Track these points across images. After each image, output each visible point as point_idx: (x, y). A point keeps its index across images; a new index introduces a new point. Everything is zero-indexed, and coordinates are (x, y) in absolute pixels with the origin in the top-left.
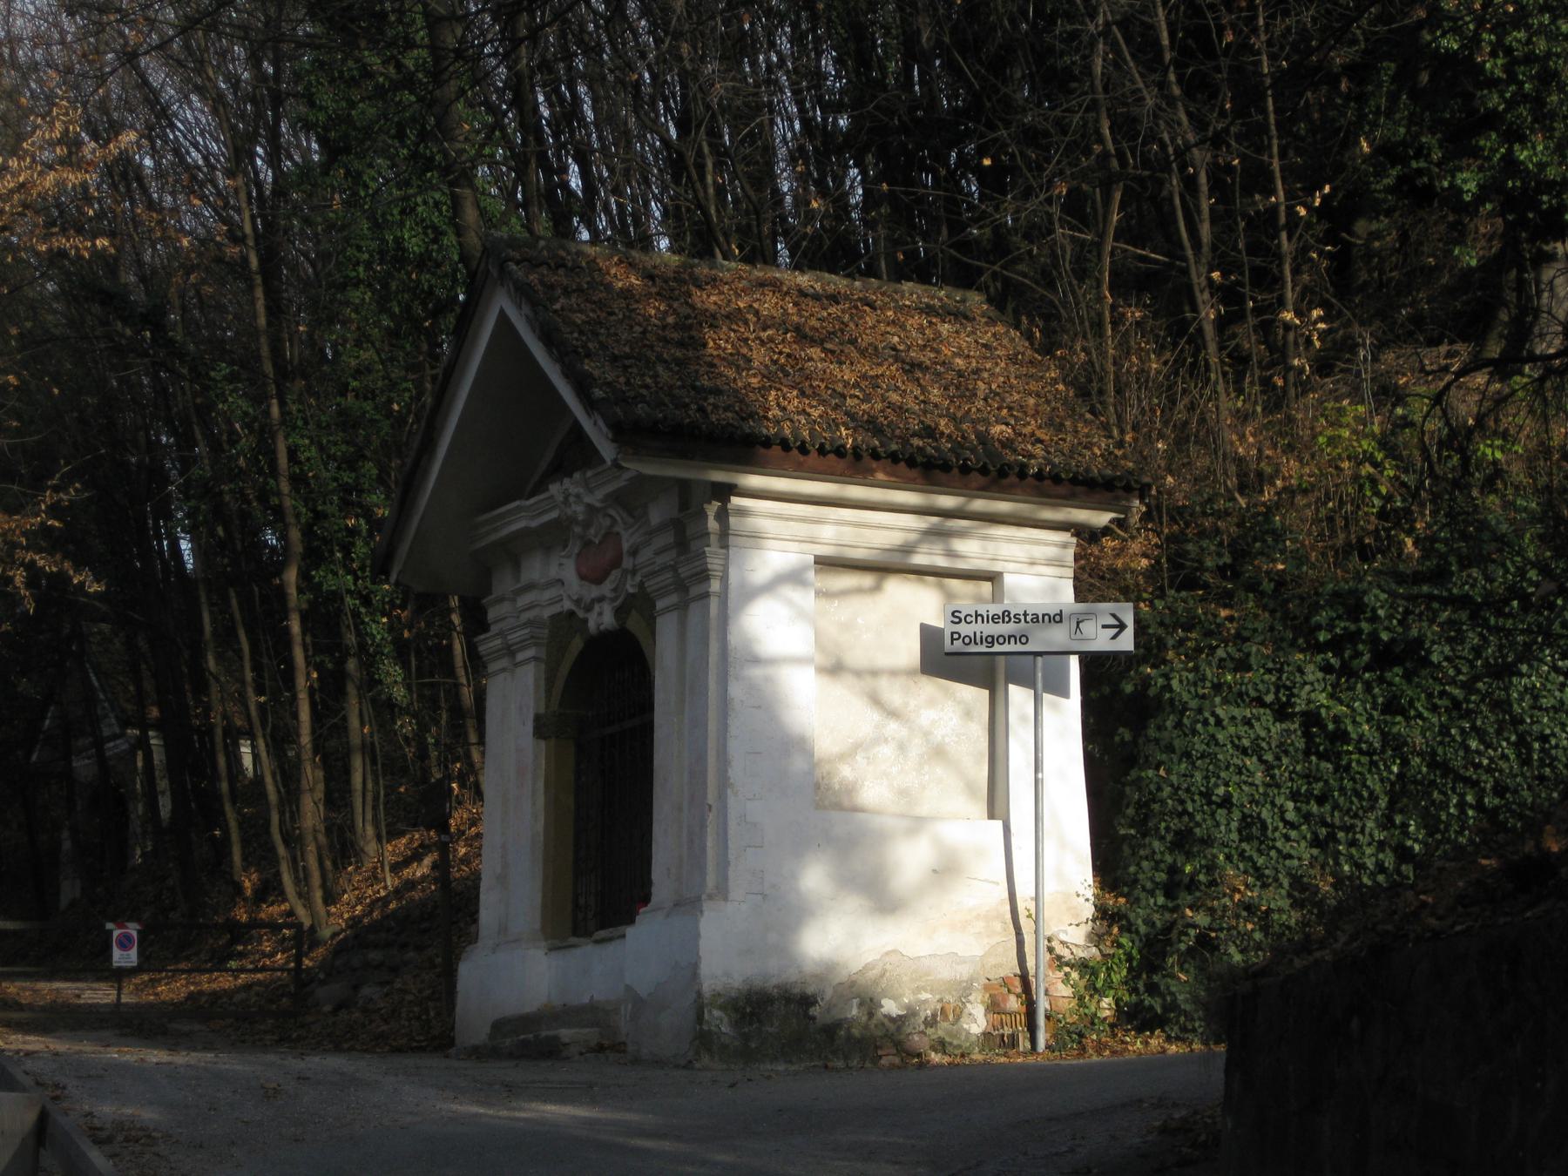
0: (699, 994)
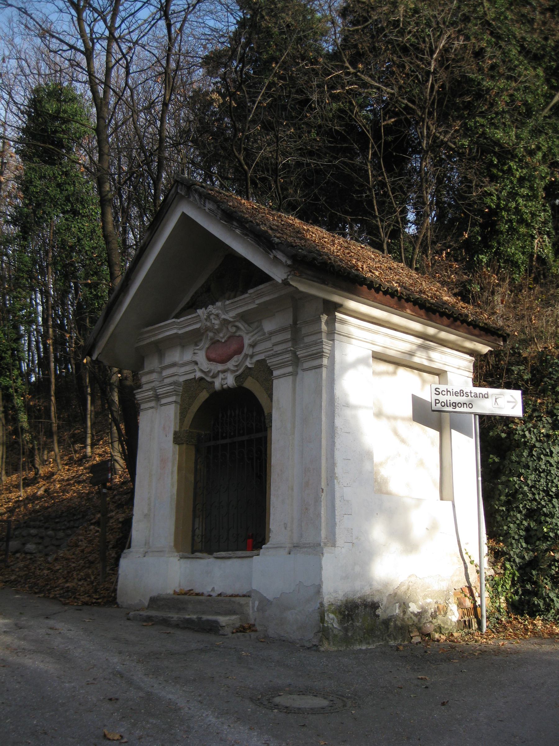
0: (322, 604)
